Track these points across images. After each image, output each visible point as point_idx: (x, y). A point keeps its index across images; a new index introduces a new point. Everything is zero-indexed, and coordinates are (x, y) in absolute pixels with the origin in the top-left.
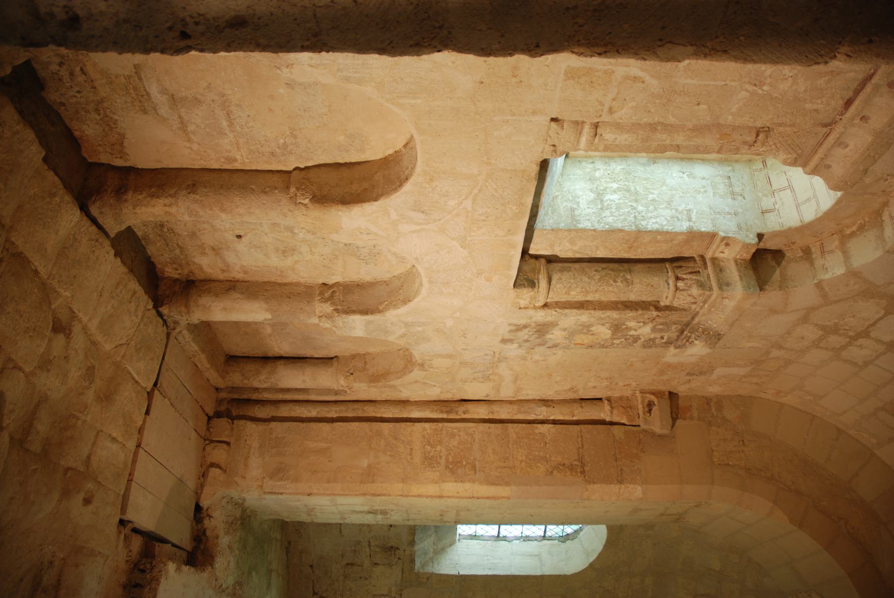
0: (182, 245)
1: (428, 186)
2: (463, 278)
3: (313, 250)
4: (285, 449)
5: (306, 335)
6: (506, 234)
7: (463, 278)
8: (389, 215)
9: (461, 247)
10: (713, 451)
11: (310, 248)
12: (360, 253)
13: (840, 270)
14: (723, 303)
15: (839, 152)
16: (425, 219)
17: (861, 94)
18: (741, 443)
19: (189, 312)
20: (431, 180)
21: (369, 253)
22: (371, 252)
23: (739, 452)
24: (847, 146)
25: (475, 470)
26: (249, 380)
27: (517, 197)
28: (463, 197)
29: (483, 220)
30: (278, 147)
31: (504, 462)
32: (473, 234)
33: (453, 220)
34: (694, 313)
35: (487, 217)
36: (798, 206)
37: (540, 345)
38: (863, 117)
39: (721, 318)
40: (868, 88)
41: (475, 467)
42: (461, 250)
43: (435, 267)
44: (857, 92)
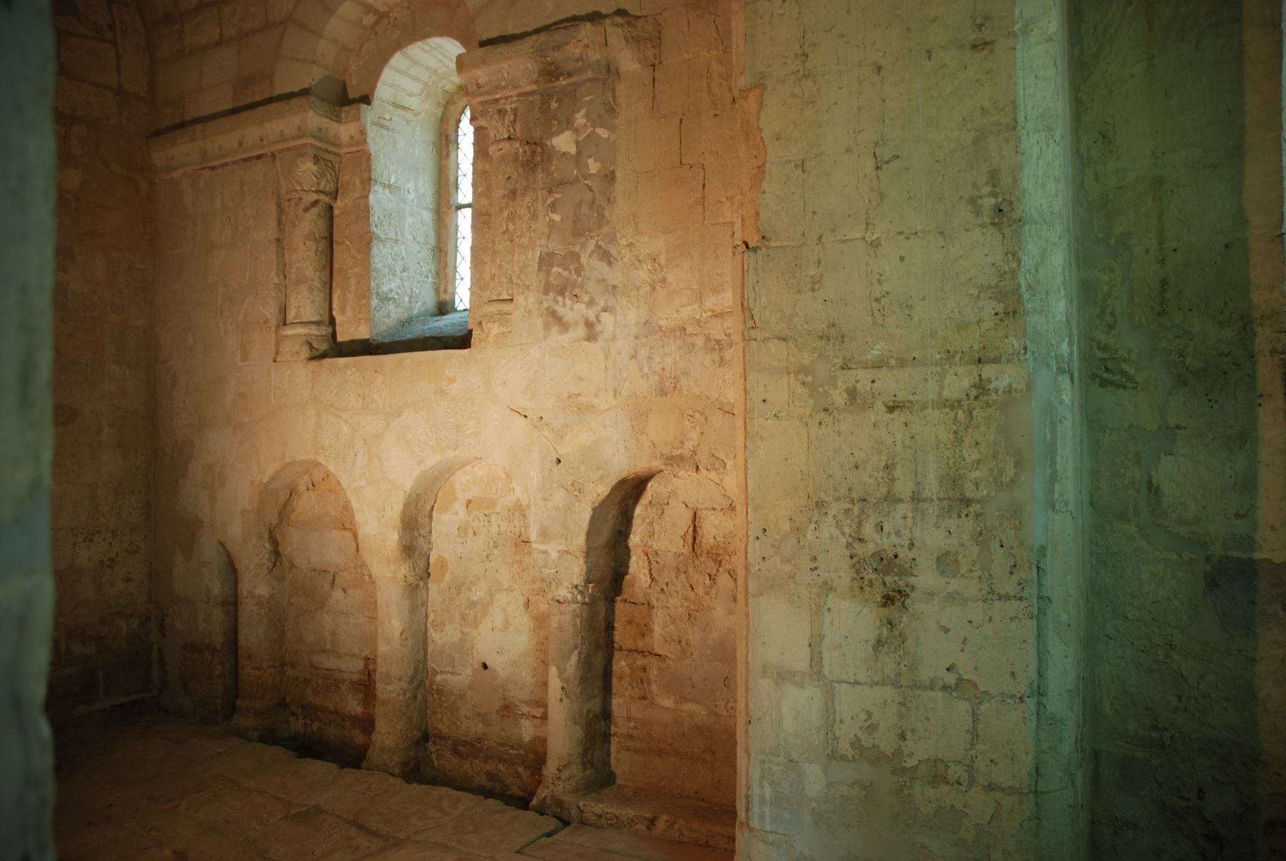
1: (329, 451)
2: (449, 411)
3: (504, 587)
6: (380, 373)
7: (449, 411)
8: (361, 487)
9: (399, 416)
11: (502, 590)
12: (509, 532)
15: (288, 133)
16: (364, 454)
20: (323, 448)
21: (510, 522)
22: (506, 519)
27: (338, 373)
28: (339, 419)
29: (363, 399)
32: (381, 406)
33: (364, 427)
35: (359, 395)
37: (813, 276)
39: (509, 65)
42: (404, 416)
43: (431, 443)
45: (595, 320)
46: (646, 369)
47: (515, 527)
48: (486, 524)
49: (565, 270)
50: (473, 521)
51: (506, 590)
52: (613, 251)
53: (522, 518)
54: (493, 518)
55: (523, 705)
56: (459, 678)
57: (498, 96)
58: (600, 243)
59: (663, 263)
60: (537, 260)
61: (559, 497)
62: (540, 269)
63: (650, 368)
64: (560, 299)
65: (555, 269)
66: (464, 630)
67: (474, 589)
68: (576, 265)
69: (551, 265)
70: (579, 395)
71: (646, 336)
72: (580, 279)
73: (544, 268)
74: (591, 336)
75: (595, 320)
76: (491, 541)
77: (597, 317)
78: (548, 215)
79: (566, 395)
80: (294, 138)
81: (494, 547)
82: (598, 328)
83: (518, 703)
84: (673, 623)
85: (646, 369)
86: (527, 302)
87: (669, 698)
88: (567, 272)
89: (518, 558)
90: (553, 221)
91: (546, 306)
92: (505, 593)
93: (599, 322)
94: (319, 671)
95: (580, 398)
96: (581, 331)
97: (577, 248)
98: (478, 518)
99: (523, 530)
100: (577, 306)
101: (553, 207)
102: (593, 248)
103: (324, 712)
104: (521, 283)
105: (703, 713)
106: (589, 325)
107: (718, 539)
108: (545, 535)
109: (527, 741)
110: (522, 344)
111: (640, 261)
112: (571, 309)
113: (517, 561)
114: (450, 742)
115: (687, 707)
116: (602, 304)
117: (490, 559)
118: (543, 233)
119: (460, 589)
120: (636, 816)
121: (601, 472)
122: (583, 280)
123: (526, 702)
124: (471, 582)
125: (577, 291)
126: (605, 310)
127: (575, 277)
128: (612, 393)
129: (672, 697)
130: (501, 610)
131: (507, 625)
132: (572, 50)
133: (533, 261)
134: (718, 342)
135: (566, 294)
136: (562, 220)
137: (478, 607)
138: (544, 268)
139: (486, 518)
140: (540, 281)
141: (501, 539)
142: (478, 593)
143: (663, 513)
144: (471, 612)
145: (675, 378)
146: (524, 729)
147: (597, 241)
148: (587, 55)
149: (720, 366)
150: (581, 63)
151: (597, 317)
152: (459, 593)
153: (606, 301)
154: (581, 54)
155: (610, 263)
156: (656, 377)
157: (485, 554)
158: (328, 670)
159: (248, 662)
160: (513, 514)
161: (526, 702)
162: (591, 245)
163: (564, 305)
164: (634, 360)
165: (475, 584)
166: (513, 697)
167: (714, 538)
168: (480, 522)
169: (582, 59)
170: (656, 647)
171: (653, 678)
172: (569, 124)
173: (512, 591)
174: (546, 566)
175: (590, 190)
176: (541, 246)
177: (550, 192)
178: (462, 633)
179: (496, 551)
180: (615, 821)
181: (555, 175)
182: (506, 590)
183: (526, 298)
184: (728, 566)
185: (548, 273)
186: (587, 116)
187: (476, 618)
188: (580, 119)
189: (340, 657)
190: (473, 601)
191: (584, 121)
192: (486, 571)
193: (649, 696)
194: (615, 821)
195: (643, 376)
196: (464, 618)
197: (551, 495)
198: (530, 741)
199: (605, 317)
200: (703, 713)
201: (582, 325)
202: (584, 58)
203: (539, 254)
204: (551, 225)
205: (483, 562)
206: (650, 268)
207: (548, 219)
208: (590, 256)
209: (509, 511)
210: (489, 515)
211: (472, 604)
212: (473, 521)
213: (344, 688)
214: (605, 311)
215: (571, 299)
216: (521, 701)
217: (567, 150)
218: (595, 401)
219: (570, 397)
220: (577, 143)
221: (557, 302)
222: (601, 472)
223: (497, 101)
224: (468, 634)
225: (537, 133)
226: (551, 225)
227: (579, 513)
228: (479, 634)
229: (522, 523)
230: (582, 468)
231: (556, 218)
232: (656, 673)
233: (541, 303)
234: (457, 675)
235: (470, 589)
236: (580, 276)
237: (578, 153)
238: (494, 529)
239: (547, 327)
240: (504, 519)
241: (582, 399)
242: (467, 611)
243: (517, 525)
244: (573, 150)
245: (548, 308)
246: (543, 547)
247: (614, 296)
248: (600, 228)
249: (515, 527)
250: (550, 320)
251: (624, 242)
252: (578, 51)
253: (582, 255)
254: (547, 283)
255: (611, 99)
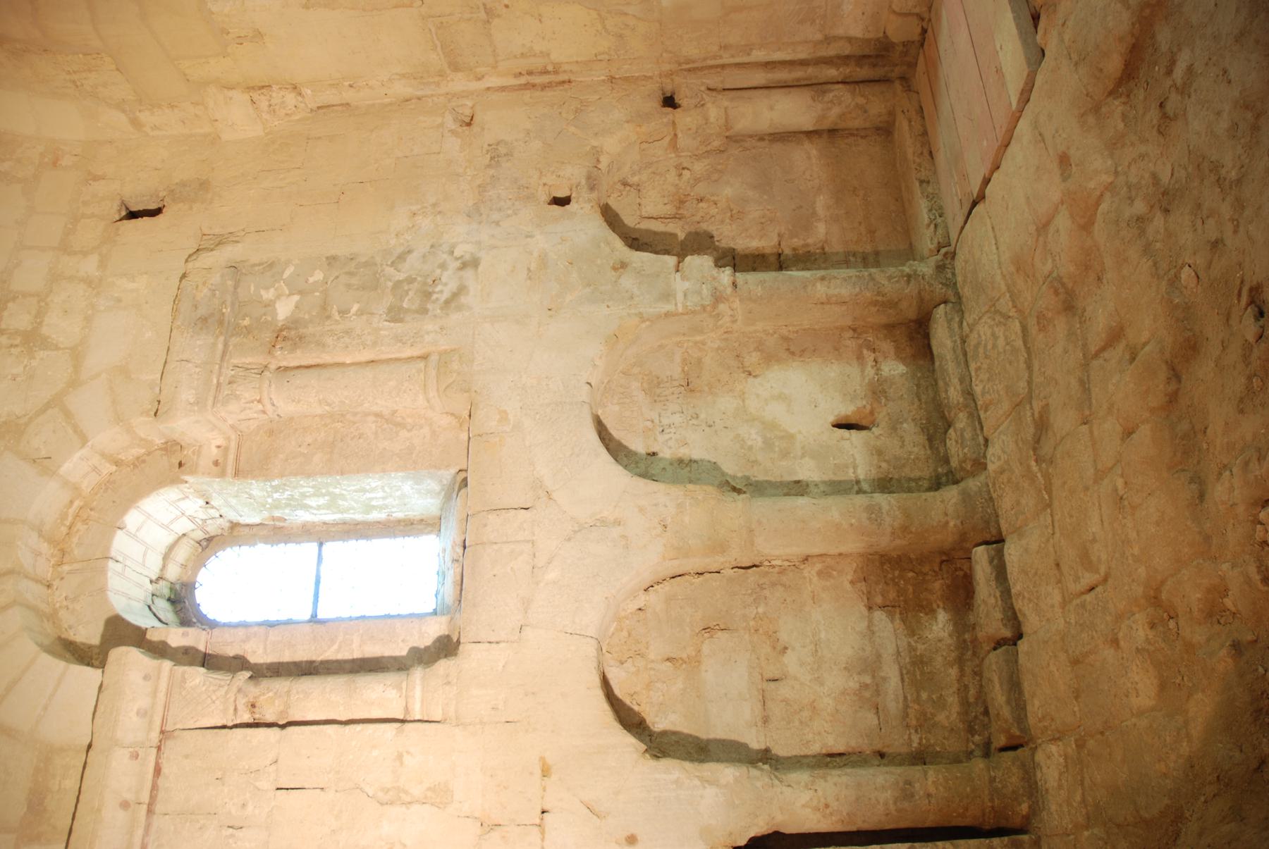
0: (916, 400)
3: (741, 403)
4: (797, 7)
5: (765, 197)
7: (538, 416)
10: (118, 70)
11: (744, 407)
13: (66, 467)
14: (194, 392)
15: (143, 702)
17: (150, 786)
18: (79, 84)
19: (919, 293)
23: (74, 72)
24: (138, 713)
25: (485, 8)
26: (857, 104)
30: (766, 598)
31: (442, 23)
34: (227, 358)
36: (149, 516)
38: (137, 758)
40: (145, 797)
41: (486, 12)
44: (154, 787)
45: (460, 261)
46: (510, 212)
47: (673, 393)
48: (673, 430)
49: (407, 294)
50: (670, 448)
51: (743, 401)
52: (399, 250)
53: (661, 386)
54: (665, 421)
55: (866, 374)
56: (858, 456)
57: (215, 381)
58: (389, 263)
59: (419, 207)
60: (393, 324)
61: (627, 282)
62: (401, 321)
63: (509, 208)
64: (435, 296)
65: (405, 305)
66: (799, 454)
67: (749, 443)
68: (405, 284)
69: (400, 309)
70: (529, 269)
71: (481, 214)
72: (419, 279)
73: (402, 316)
74: (474, 263)
75: (460, 261)
76: (691, 422)
77: (457, 259)
78: (351, 317)
79: (529, 281)
80: (155, 693)
81: (697, 418)
82: (467, 257)
83: (867, 381)
84: (747, 230)
85: (510, 212)
86: (432, 332)
87: (816, 227)
88: (410, 293)
89: (706, 389)
90: (358, 310)
91: (439, 311)
92: (747, 402)
93: (462, 257)
94: (909, 698)
95: (532, 269)
96: (469, 274)
97: (390, 284)
98: (667, 441)
99: (676, 383)
100: (444, 279)
101: (343, 312)
102: (392, 269)
103: (966, 687)
104: (412, 340)
105: (822, 198)
106: (464, 266)
107: (666, 202)
108: (667, 296)
109: (904, 368)
110: (474, 334)
111: (413, 226)
112: (446, 284)
113: (710, 389)
114: (940, 470)
115: (821, 211)
116: (445, 256)
117: (712, 423)
118: (367, 320)
119: (753, 462)
120: (922, 193)
121: (602, 245)
122: (421, 276)
123: (863, 371)
124: (742, 447)
125: (430, 281)
126: (452, 253)
127: (416, 284)
128: (529, 239)
129: (815, 224)
130: (767, 405)
131: (781, 397)
132: (202, 295)
133: (392, 328)
134: (492, 158)
135: (431, 290)
136: (358, 302)
137: (768, 436)
138: (402, 316)
139: (666, 431)
140: (413, 319)
141: (687, 409)
142: (754, 436)
143: (646, 244)
144: (777, 444)
145: (519, 189)
146: (892, 372)
147: (387, 265)
148: (212, 284)
149: (512, 156)
150: (217, 292)
151: (457, 259)
152: (755, 462)
153: (443, 253)
154: (210, 289)
155: (410, 252)
156: (517, 203)
157: (707, 429)
158: (903, 680)
159: (917, 785)
160: (659, 396)
161: (863, 371)
162: (390, 270)
163: (441, 292)
164: (501, 223)
165: (743, 440)
166: (861, 385)
167: (665, 204)
168: (671, 438)
169: (214, 290)
170: (772, 244)
171: (802, 242)
172: (270, 305)
173: (744, 393)
174: (699, 293)
175: (337, 277)
176: (379, 322)
177: (329, 317)
178: (803, 456)
179: (702, 416)
180: (934, 211)
181: (314, 314)
182: (743, 401)
183: (428, 333)
184: (689, 188)
185: (407, 311)
186: (267, 288)
187: (782, 438)
188: (268, 295)
189: (879, 656)
190: (763, 442)
191: (272, 290)
192: (725, 427)
193: (821, 244)
194: (934, 211)
195: (516, 214)
196: (785, 454)
197: (627, 292)
198: (904, 365)
199: (457, 253)
200: (822, 198)
201: (462, 273)
202: (214, 288)
203: (387, 323)
204: (360, 313)
205: (716, 431)
206: (421, 217)
207: (354, 317)
208: (399, 271)
209: (655, 401)
210: (662, 426)
211: (768, 444)
212: (670, 448)
213: (921, 648)
214: (453, 252)
215: (437, 285)
216: (863, 377)
217: (294, 304)
218: (536, 254)
219: (530, 278)
220: (291, 294)
221: (437, 299)
222: (602, 245)
223: (219, 384)
224: (803, 448)
225: (268, 336)
226: (360, 313)
227: (642, 262)
228: (800, 432)
229: (668, 384)
230: (599, 262)
231: (355, 308)
232: (796, 240)
233: (435, 316)
234: (855, 459)
235: (751, 448)
236: (415, 279)
237: (300, 292)
238: (677, 419)
239: (459, 308)
240: (665, 407)
241: (533, 266)
242: (777, 449)
243: (671, 390)
244: (296, 298)
245: (442, 309)
246: (680, 296)
247: (441, 245)
248: (376, 264)
249: (673, 393)
250: (453, 305)
251: (393, 242)
252: (205, 291)
253: (397, 278)
254: (417, 312)
255: (261, 267)
